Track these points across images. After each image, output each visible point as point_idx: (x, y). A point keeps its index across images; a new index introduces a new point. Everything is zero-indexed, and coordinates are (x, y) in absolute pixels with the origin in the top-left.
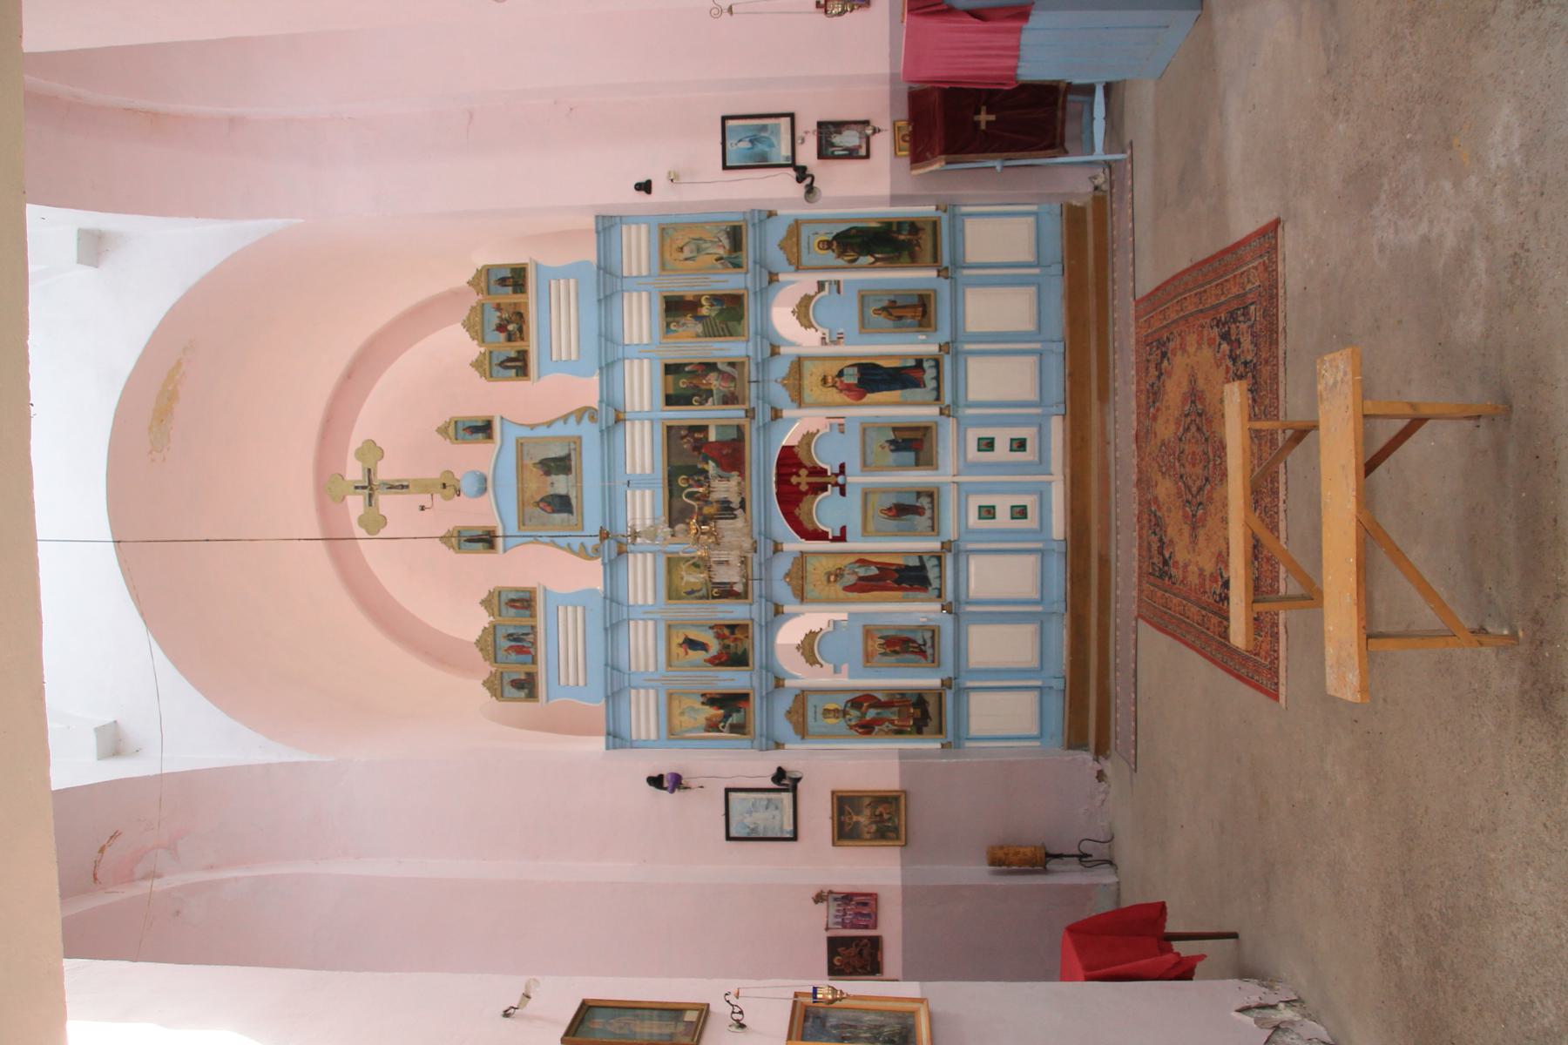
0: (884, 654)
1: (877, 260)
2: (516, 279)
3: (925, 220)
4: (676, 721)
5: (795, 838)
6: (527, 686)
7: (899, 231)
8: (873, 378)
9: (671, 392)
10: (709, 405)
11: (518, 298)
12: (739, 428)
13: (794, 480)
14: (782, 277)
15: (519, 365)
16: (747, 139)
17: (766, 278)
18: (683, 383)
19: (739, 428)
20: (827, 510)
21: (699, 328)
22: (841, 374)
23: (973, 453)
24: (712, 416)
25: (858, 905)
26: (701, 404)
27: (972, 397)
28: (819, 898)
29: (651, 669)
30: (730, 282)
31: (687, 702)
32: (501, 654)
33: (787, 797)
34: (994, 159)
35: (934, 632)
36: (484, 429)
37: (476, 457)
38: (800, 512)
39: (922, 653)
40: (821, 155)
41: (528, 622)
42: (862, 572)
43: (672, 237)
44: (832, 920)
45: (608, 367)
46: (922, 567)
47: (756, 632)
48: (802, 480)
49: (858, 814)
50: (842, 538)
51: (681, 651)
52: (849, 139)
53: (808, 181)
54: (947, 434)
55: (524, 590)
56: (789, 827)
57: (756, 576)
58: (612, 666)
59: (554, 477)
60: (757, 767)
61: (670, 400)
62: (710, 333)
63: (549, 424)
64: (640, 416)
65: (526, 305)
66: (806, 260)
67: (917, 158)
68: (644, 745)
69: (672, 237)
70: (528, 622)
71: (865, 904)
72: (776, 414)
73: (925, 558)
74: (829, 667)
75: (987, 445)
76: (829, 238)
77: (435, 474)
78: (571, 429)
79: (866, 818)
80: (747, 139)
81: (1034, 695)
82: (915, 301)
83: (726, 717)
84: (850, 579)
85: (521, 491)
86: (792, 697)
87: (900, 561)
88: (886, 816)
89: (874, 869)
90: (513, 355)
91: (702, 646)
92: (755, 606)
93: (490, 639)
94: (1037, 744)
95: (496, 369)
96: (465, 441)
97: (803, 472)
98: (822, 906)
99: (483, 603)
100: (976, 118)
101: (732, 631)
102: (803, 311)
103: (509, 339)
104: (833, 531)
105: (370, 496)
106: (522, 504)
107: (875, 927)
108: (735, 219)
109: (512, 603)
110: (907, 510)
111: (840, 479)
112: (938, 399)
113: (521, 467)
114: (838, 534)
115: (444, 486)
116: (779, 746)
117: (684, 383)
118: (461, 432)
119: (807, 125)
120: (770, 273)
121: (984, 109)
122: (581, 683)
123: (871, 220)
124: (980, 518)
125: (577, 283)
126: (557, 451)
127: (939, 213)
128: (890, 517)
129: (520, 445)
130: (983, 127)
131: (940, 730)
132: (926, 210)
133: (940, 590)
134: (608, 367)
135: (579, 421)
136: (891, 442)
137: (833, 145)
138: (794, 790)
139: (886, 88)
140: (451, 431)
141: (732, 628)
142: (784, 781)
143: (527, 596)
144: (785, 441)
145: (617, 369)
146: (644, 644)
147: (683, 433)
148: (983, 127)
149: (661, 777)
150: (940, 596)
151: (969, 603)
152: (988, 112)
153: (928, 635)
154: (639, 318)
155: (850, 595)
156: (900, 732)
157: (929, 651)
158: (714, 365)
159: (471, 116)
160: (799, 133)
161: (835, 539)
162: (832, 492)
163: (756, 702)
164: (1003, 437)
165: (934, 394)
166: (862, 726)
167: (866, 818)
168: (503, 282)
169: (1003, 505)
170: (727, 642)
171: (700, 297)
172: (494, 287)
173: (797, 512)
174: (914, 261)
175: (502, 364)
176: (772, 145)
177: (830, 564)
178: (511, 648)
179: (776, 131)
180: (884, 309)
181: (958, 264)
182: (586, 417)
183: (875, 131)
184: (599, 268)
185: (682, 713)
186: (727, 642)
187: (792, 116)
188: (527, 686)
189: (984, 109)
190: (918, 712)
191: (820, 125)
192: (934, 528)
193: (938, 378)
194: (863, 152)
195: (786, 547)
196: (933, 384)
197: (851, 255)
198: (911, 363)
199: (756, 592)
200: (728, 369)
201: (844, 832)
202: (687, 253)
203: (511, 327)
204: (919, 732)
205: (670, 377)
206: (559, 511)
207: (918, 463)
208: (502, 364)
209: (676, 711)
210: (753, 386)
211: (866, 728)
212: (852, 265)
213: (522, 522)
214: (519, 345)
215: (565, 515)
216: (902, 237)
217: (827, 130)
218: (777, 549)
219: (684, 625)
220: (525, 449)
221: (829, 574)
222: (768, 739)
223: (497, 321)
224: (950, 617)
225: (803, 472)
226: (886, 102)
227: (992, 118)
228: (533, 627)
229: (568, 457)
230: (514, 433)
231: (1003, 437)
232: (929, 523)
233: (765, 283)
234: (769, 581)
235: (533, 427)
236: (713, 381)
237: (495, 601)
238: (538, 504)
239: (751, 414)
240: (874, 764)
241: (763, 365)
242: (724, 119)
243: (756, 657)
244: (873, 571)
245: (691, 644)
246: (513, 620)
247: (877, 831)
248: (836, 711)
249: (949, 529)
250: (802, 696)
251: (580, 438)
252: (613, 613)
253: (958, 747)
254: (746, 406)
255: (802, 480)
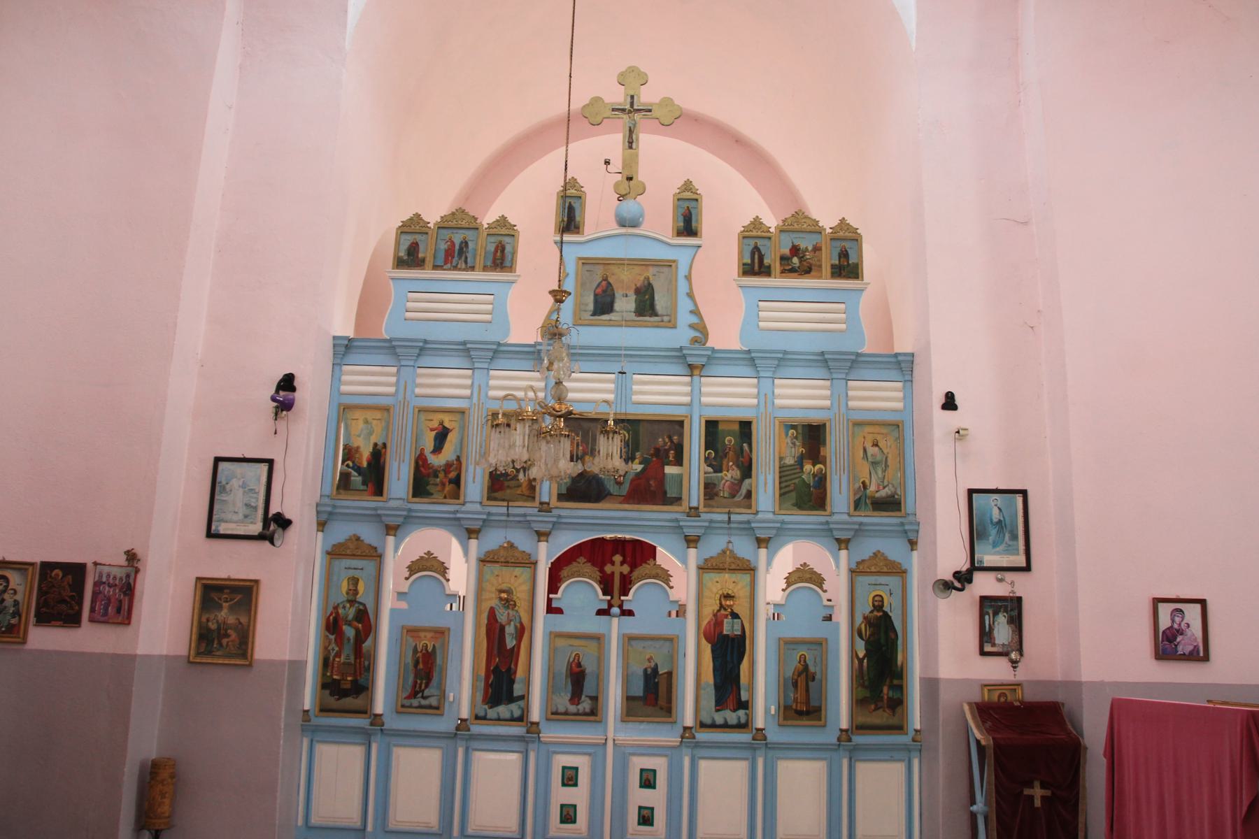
0: (415, 650)
1: (861, 661)
2: (847, 268)
3: (904, 716)
4: (358, 414)
5: (210, 534)
6: (410, 258)
7: (892, 687)
8: (728, 650)
9: (721, 427)
10: (703, 466)
11: (826, 269)
12: (677, 500)
13: (618, 558)
14: (844, 553)
15: (755, 266)
16: (1001, 518)
17: (843, 535)
18: (729, 440)
19: (677, 500)
20: (582, 594)
21: (790, 461)
22: (735, 616)
23: (640, 762)
24: (693, 470)
25: (119, 601)
26: (706, 459)
27: (703, 764)
28: (132, 557)
29: (418, 391)
30: (839, 496)
31: (378, 427)
32: (446, 234)
33: (257, 528)
34: (987, 803)
35: (437, 709)
36: (688, 227)
37: (659, 217)
38: (581, 564)
39: (414, 695)
40: (983, 599)
41: (479, 262)
42: (510, 630)
43: (891, 432)
44: (106, 569)
45: (750, 360)
46: (511, 699)
47: (449, 508)
48: (617, 567)
49: (231, 608)
50: (551, 609)
51: (435, 424)
52: (1002, 633)
53: (957, 584)
54: (666, 736)
55: (513, 260)
56: (223, 529)
57: (512, 511)
58: (424, 348)
59: (633, 297)
60: (298, 494)
61: (712, 426)
62: (784, 473)
63: (690, 295)
64: (695, 393)
65: (820, 277)
66: (863, 580)
67: (984, 711)
68: (336, 379)
69: (891, 432)
70: (479, 262)
71: (119, 611)
72: (691, 541)
73: (521, 703)
74: (405, 586)
75: (648, 780)
76: (886, 608)
77: (642, 175)
78: (684, 318)
79: (224, 614)
80: (1001, 518)
81: (358, 824)
82: (814, 703)
83: (358, 469)
84: (502, 616)
85: (620, 262)
86: (374, 544)
87: (520, 674)
88: (225, 641)
89: (162, 622)
90: (766, 261)
91: (438, 449)
92: (478, 507)
93: (464, 224)
94: (300, 822)
95: (752, 242)
96: (676, 208)
97: (626, 569)
98: (122, 560)
99: (504, 218)
100: (1037, 784)
101: (454, 481)
102: (805, 576)
103: (783, 258)
104: (560, 598)
105: (623, 110)
106: (606, 263)
107: (92, 620)
108: (908, 506)
109: (501, 248)
110: (578, 683)
111: (615, 610)
112: (703, 725)
113: (646, 263)
114: (554, 605)
115: (630, 179)
116: (321, 526)
117: (730, 441)
118: (686, 204)
119: (1020, 585)
120: (847, 541)
121: (1048, 793)
122: (408, 315)
123: (905, 658)
124: (564, 768)
125: (841, 331)
126: (660, 303)
127: (911, 733)
128: (570, 665)
129: (670, 264)
130: (1027, 792)
131: (325, 710)
132: (915, 718)
133: (484, 718)
134: (750, 360)
135: (692, 326)
136: (655, 670)
137: (996, 614)
138: (261, 537)
139: (1059, 677)
140: (687, 195)
141: (457, 482)
142: (275, 525)
143: (507, 264)
144: (659, 549)
145: (748, 371)
146: (447, 384)
147: (675, 438)
148: (1027, 792)
149: (293, 389)
150: (477, 718)
151: (467, 749)
152: (1043, 797)
153: (433, 701)
154: (802, 396)
155: (485, 615)
156: (326, 663)
157: (415, 702)
158: (750, 476)
159: (1025, 223)
160: (1009, 576)
161: (549, 601)
162: (601, 600)
163: (371, 503)
164: (655, 798)
165: (709, 721)
166: (336, 620)
167: (224, 614)
168: (844, 254)
169: (578, 796)
170: (441, 475)
171: (824, 464)
172: (839, 244)
173: (582, 560)
174: (859, 703)
175: (756, 249)
176: (995, 545)
177: (521, 594)
178: (453, 244)
179: (1012, 551)
180: (806, 667)
181: (855, 754)
182: (697, 334)
183: (1014, 663)
184: (858, 355)
185: (366, 422)
186: (441, 475)
187: (1027, 568)
188: (410, 258)
189: (1048, 793)
190: (348, 686)
191: (1019, 599)
192: (555, 715)
193: (726, 726)
194: (988, 648)
195: (543, 546)
196: (719, 721)
197: (867, 632)
198: (744, 696)
199: (494, 510)
200: (744, 491)
201: (212, 593)
202: (872, 450)
203: (795, 260)
204: (324, 686)
205: (736, 427)
206: (596, 302)
207: (629, 699)
208: (756, 249)
209: (370, 415)
210: (725, 517)
211: (333, 625)
212: (856, 632)
213: (586, 262)
214: (777, 267)
215: (591, 307)
216: (885, 689)
217: (1012, 608)
218: (542, 535)
219: (463, 428)
220: (666, 270)
221: (509, 592)
222: (330, 513)
223: (803, 246)
224: (452, 728)
225: (626, 569)
226: (1044, 676)
227: (1038, 803)
228: (473, 268)
229: (654, 313)
230: (683, 258)
231: (655, 798)
232: (562, 709)
233: (838, 535)
234: (506, 524)
235: (688, 278)
236: (731, 474)
237: (504, 231)
238: (605, 279)
239: (694, 512)
240: (289, 628)
241: (747, 528)
242: (1024, 493)
243: (422, 506)
244: (510, 643)
245: (442, 435)
246: (482, 247)
247: (209, 630)
248: (356, 592)
249: (550, 733)
250: (375, 555)
251: (674, 327)
252: (483, 353)
253: (304, 730)
254: (701, 508)
255: (617, 567)
